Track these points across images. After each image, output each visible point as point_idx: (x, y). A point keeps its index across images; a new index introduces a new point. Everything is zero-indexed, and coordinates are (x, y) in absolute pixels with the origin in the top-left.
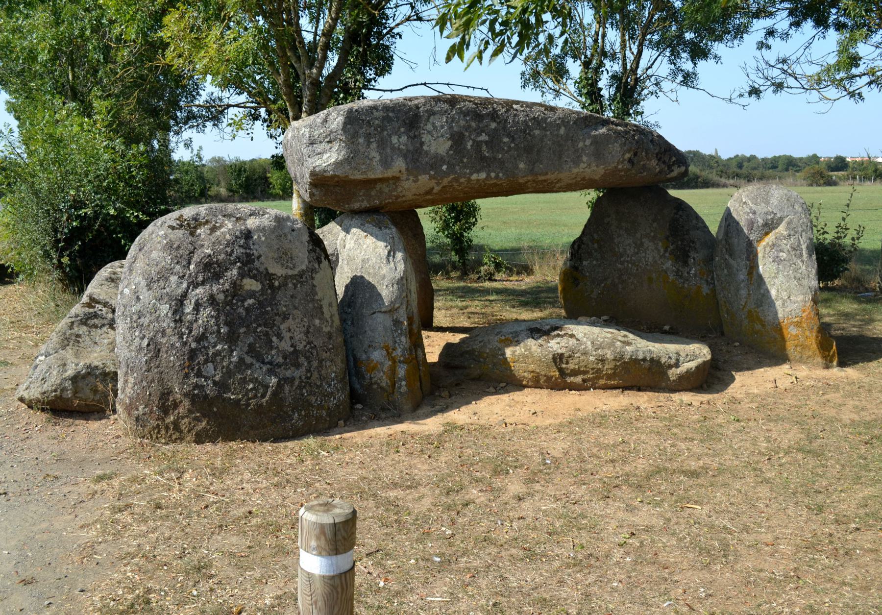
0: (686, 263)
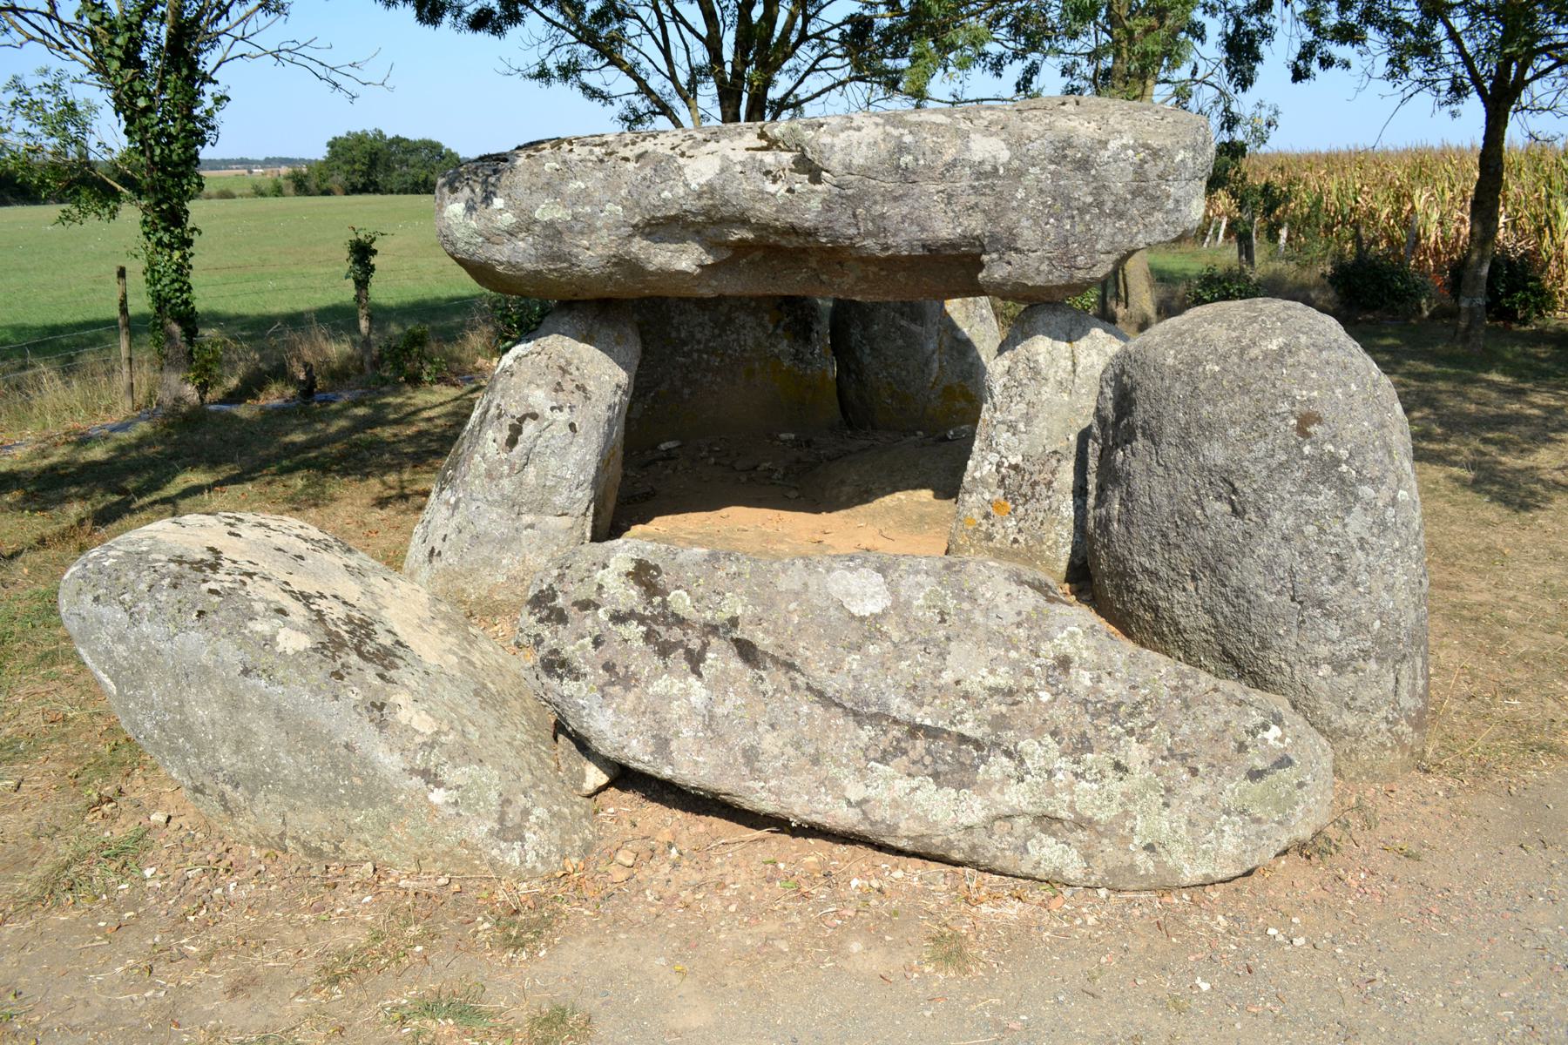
0: (808, 340)
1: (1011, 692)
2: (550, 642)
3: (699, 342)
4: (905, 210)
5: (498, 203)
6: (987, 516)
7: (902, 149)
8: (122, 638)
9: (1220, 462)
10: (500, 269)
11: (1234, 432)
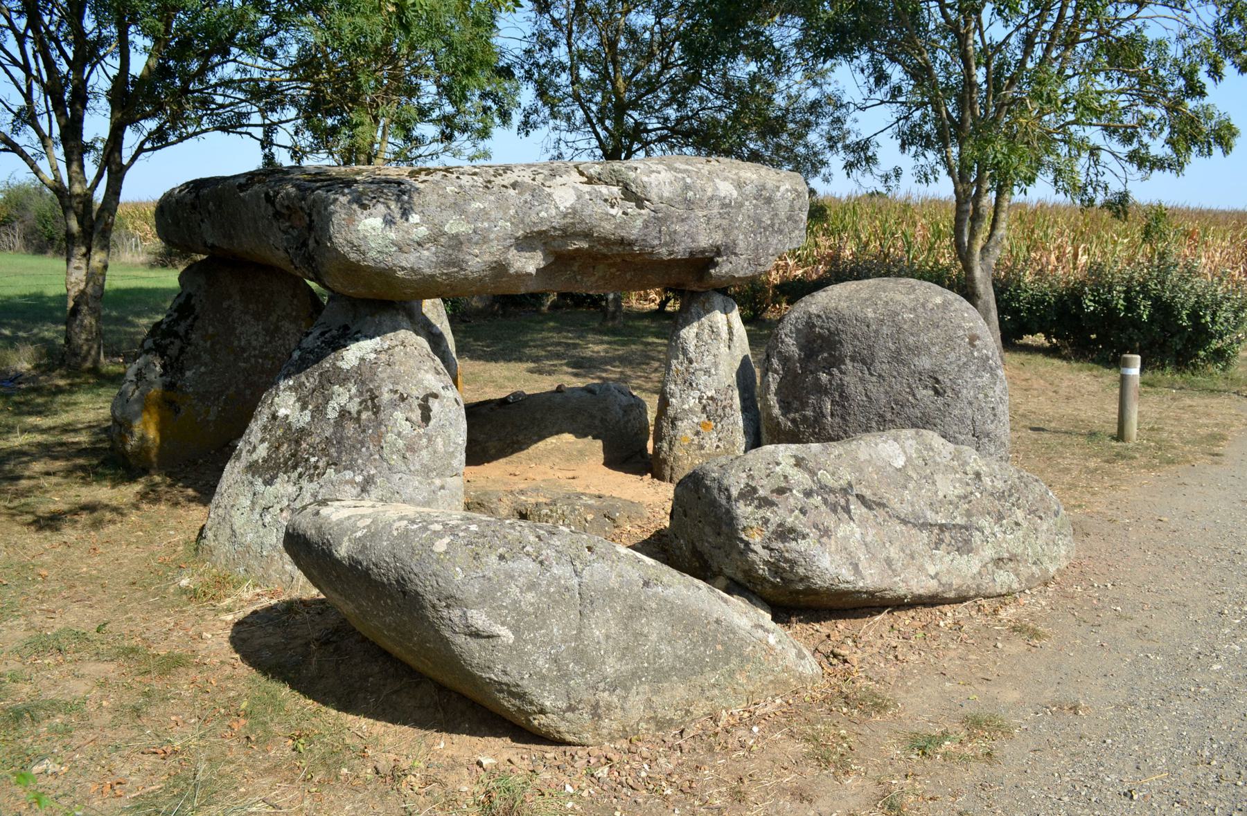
1: (966, 497)
2: (774, 520)
3: (255, 349)
4: (687, 227)
5: (415, 218)
6: (697, 433)
7: (687, 187)
8: (532, 586)
9: (927, 366)
10: (400, 274)
11: (934, 349)
